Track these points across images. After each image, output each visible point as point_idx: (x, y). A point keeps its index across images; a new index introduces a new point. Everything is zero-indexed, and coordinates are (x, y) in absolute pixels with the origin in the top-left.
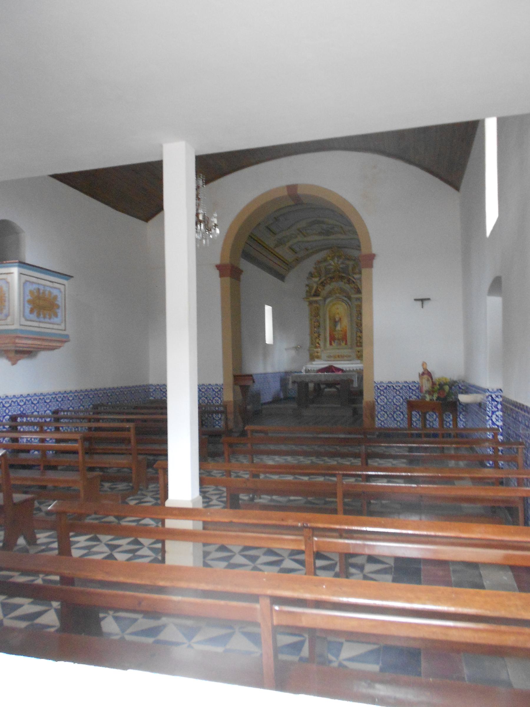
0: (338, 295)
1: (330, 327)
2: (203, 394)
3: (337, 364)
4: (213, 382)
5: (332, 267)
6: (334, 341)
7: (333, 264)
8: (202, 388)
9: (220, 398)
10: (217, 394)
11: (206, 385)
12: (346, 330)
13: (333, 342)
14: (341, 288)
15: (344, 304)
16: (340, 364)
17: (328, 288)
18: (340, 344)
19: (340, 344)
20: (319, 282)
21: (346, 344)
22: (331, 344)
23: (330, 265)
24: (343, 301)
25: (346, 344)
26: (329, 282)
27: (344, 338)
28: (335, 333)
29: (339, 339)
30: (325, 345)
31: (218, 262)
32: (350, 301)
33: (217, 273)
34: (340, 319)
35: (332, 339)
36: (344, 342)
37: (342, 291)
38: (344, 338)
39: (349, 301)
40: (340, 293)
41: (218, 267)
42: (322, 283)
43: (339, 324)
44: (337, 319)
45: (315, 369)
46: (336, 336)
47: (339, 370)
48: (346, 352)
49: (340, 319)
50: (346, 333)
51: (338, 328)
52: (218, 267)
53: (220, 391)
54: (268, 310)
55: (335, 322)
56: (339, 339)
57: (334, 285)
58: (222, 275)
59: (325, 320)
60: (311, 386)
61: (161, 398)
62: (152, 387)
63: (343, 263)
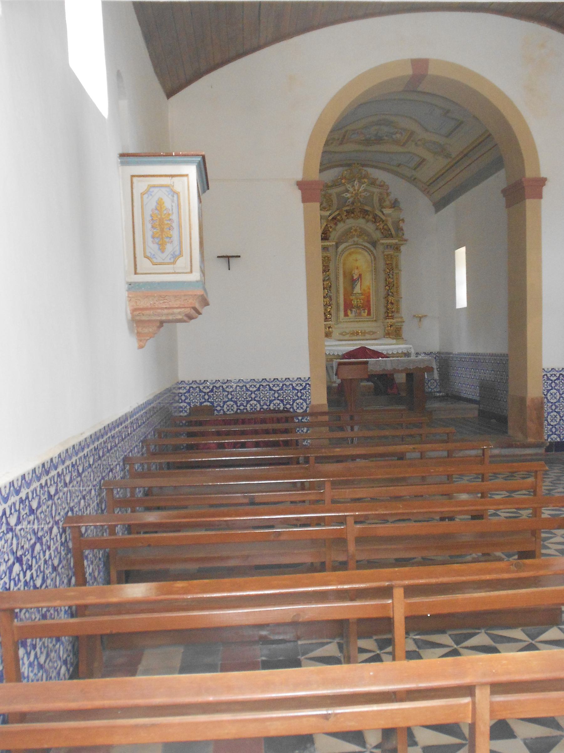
0: (356, 239)
1: (345, 289)
2: (206, 397)
3: (373, 345)
4: (293, 375)
5: (349, 195)
6: (351, 310)
7: (351, 190)
8: (274, 386)
9: (305, 400)
10: (299, 394)
11: (256, 380)
12: (369, 293)
13: (349, 312)
14: (361, 228)
15: (366, 254)
16: (377, 345)
17: (341, 227)
18: (360, 314)
19: (360, 314)
20: (330, 218)
21: (369, 314)
22: (346, 315)
23: (347, 191)
24: (365, 248)
25: (369, 314)
26: (344, 217)
27: (366, 306)
28: (353, 297)
29: (358, 307)
30: (338, 317)
31: (300, 177)
32: (375, 249)
33: (298, 194)
34: (360, 275)
35: (348, 306)
36: (366, 311)
37: (362, 233)
38: (366, 306)
39: (372, 249)
40: (359, 236)
41: (301, 185)
42: (334, 218)
43: (359, 284)
44: (355, 277)
45: (340, 354)
46: (355, 303)
47: (377, 354)
48: (367, 326)
49: (360, 275)
50: (369, 297)
51: (357, 290)
52: (301, 185)
53: (305, 388)
54: (461, 254)
55: (352, 281)
56: (358, 307)
57: (351, 223)
58: (305, 200)
59: (337, 278)
60: (401, 378)
61: (201, 403)
62: (185, 386)
63: (365, 190)
